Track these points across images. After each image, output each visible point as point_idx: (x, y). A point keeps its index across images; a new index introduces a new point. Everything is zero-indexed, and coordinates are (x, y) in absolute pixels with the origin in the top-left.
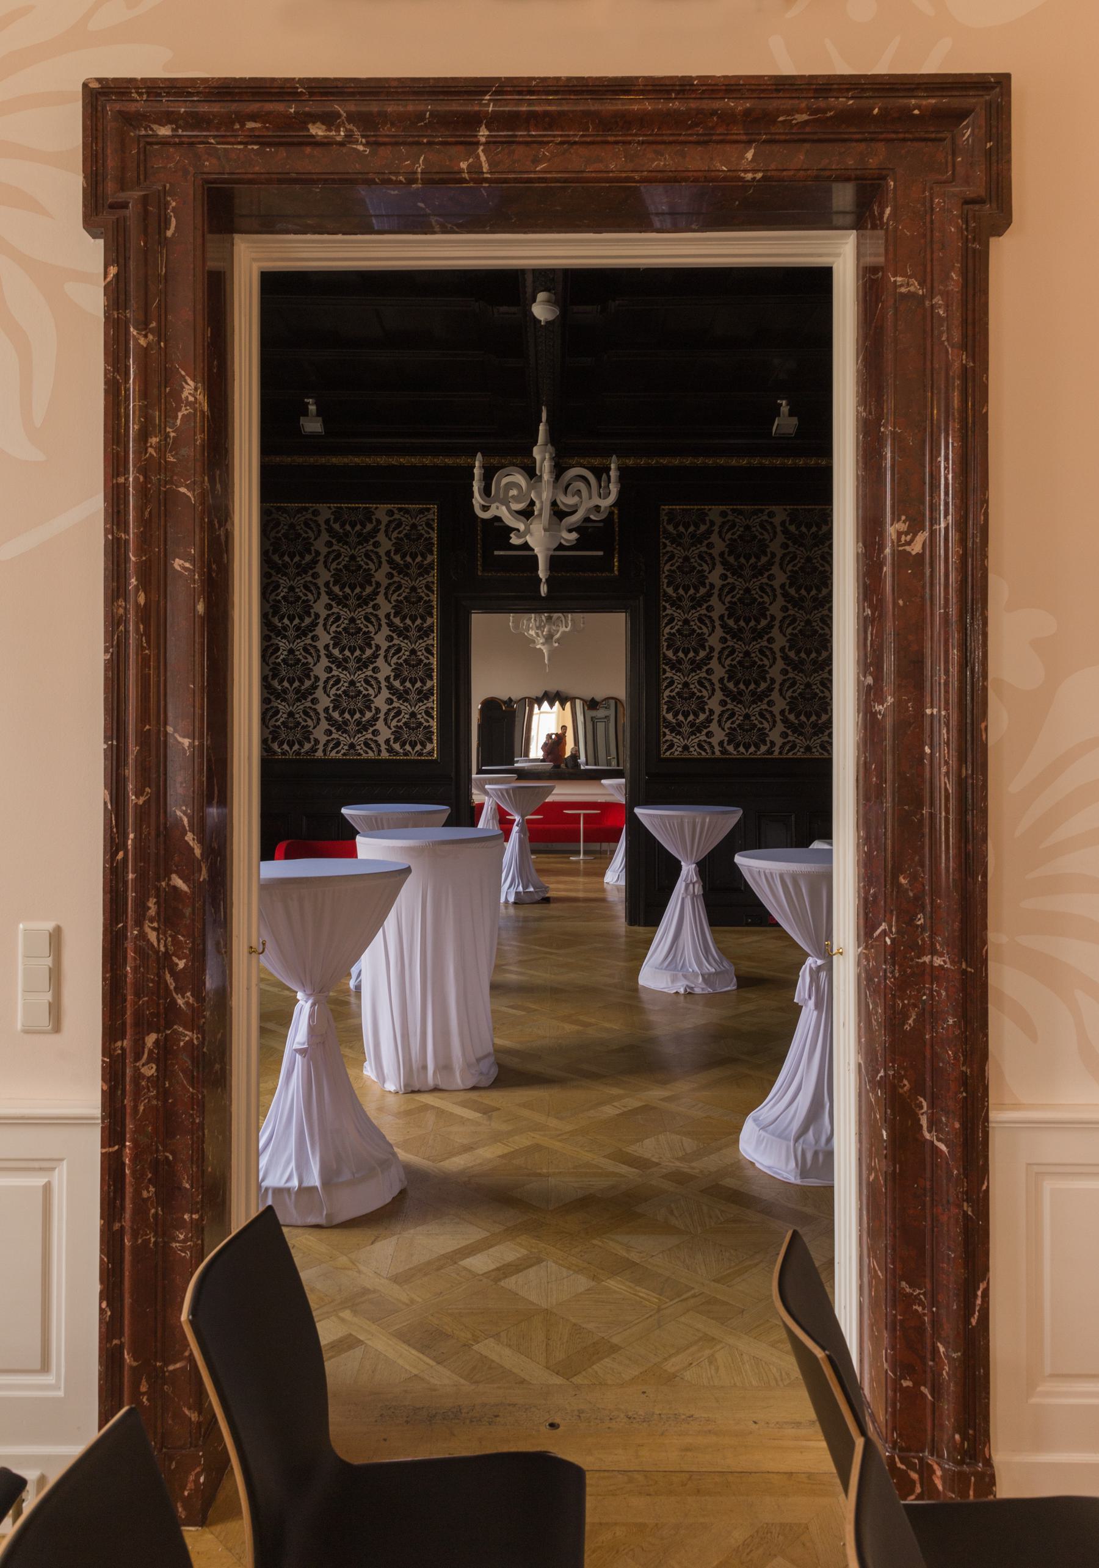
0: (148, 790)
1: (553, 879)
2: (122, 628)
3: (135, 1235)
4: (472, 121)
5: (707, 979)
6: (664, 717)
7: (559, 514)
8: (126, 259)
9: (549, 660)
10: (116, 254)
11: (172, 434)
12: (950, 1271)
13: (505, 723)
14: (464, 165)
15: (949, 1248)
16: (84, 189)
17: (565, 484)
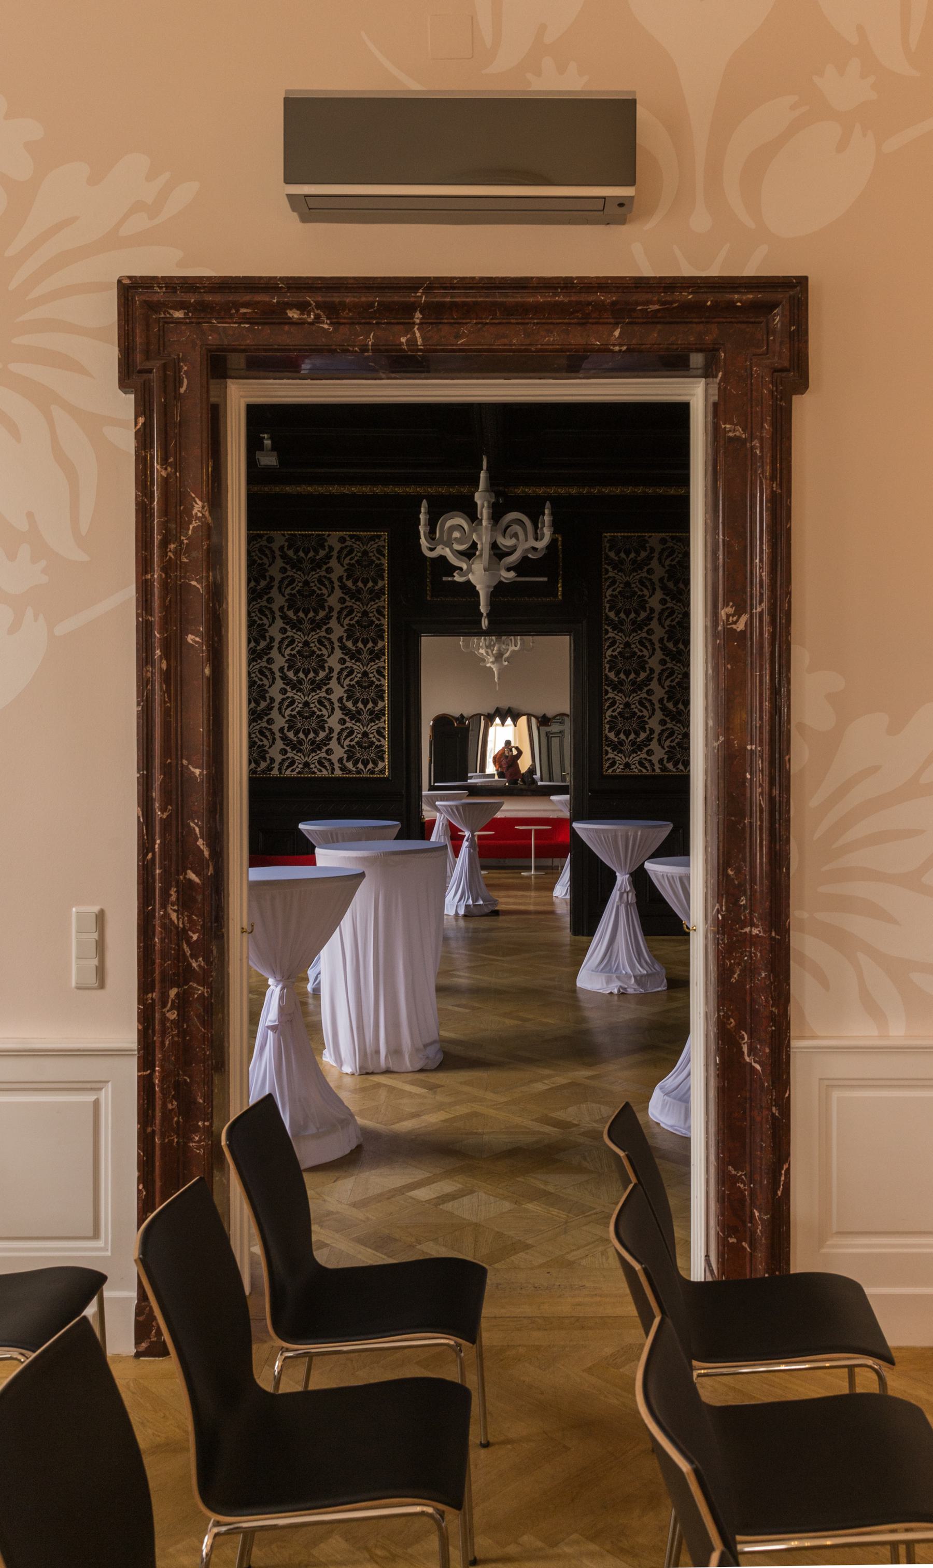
0: (169, 807)
1: (503, 893)
2: (149, 687)
3: (163, 1136)
4: (408, 309)
5: (639, 980)
6: (606, 736)
7: (498, 553)
8: (152, 411)
9: (499, 678)
10: (143, 408)
11: (185, 541)
12: (763, 1154)
13: (458, 739)
14: (403, 340)
15: (762, 1140)
16: (119, 359)
17: (504, 527)
